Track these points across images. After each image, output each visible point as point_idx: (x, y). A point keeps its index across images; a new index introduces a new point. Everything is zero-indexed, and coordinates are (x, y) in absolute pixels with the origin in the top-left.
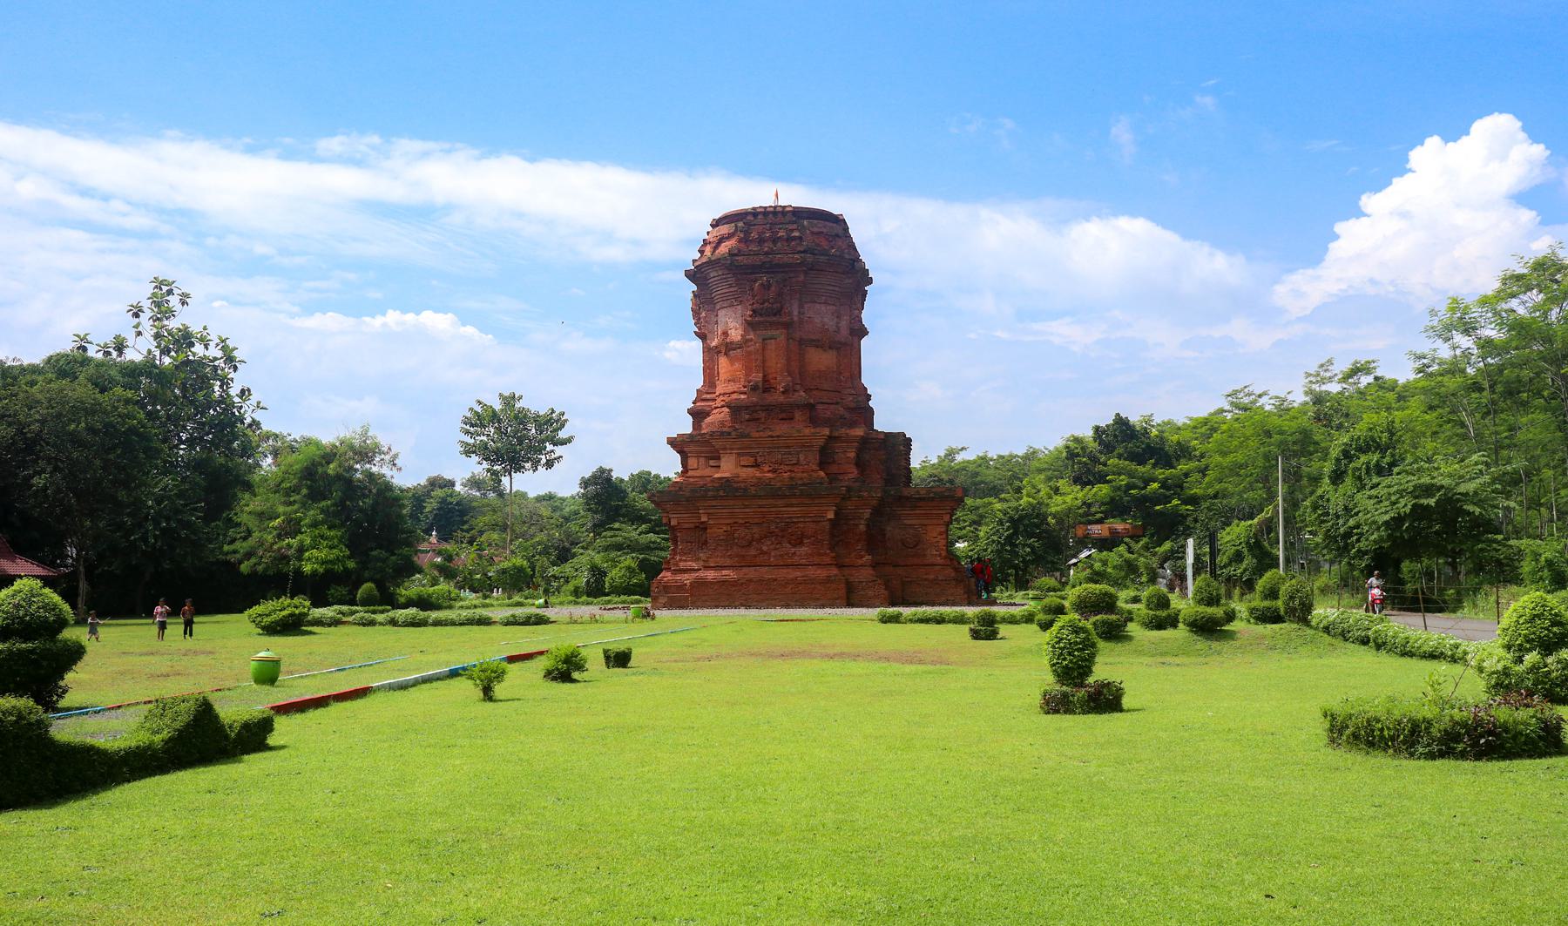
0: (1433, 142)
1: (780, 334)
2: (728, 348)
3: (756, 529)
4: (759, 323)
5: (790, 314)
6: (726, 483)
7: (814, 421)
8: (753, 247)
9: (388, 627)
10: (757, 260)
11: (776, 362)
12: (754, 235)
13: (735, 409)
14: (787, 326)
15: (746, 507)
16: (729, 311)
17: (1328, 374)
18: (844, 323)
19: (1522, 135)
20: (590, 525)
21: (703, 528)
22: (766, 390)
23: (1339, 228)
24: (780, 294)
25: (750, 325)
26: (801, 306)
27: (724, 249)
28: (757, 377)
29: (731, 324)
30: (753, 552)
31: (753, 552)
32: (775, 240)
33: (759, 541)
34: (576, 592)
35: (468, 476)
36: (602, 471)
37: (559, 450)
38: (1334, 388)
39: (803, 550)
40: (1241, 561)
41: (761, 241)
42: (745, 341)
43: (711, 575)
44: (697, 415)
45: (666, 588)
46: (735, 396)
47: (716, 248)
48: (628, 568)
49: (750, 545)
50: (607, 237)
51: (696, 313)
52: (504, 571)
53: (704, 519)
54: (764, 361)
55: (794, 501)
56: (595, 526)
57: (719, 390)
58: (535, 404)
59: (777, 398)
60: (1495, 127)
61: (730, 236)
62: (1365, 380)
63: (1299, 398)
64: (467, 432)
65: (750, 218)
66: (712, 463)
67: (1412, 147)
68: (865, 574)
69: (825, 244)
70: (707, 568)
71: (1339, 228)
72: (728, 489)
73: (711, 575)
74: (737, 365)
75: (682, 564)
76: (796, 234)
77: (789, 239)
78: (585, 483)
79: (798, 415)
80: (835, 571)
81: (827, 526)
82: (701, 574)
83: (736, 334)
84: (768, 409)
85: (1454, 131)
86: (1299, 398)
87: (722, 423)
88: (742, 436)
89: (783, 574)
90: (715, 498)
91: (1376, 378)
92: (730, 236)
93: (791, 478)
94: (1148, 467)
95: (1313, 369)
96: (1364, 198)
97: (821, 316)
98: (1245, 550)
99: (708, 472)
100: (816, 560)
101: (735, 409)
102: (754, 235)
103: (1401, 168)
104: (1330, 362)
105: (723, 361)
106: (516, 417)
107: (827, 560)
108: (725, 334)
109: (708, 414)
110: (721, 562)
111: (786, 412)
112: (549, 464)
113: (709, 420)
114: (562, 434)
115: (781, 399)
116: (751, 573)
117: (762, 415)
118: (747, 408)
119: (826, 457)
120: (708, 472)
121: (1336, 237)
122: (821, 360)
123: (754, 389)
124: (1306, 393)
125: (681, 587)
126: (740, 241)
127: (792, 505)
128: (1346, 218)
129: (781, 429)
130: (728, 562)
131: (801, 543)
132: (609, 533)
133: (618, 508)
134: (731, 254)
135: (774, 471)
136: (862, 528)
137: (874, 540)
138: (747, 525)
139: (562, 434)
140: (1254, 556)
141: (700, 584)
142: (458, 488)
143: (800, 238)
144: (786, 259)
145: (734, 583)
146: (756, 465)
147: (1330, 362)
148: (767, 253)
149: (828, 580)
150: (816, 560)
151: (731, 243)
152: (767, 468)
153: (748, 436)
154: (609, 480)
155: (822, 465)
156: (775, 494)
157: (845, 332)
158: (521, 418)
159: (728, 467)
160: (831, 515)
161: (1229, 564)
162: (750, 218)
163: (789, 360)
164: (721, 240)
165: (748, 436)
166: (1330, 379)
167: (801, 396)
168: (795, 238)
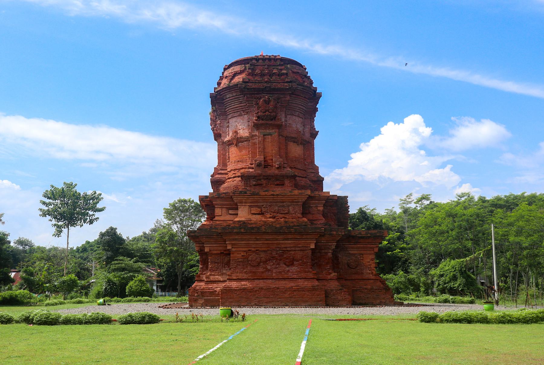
0: (391, 124)
1: (274, 132)
2: (237, 141)
3: (263, 255)
4: (262, 124)
5: (281, 119)
6: (243, 224)
7: (297, 186)
8: (258, 78)
9: (23, 325)
10: (261, 86)
11: (272, 149)
12: (258, 71)
13: (245, 178)
14: (279, 127)
15: (257, 240)
16: (239, 119)
17: (410, 200)
18: (307, 130)
19: (423, 124)
20: (105, 258)
21: (228, 253)
22: (266, 167)
23: (353, 155)
24: (276, 107)
25: (256, 126)
26: (286, 117)
27: (238, 79)
28: (260, 158)
29: (241, 126)
30: (261, 270)
31: (261, 270)
32: (271, 75)
33: (265, 262)
34: (98, 296)
35: (18, 239)
36: (112, 229)
37: (97, 215)
38: (413, 206)
39: (294, 269)
40: (456, 280)
41: (262, 75)
42: (252, 136)
43: (234, 285)
44: (216, 183)
45: (203, 293)
46: (242, 171)
47: (232, 79)
48: (140, 281)
49: (259, 265)
50: (61, 149)
51: (213, 121)
52: (64, 282)
53: (229, 247)
54: (264, 148)
55: (290, 236)
56: (108, 258)
57: (229, 168)
58: (83, 189)
59: (273, 171)
60: (414, 120)
61: (241, 72)
62: (426, 202)
63: (398, 211)
64: (44, 203)
65: (254, 61)
66: (231, 212)
67: (382, 126)
68: (334, 285)
69: (299, 79)
70: (230, 280)
71: (353, 155)
72: (245, 228)
73: (234, 285)
74: (244, 152)
75: (212, 278)
76: (285, 72)
77: (280, 75)
78: (102, 235)
79: (287, 182)
80: (316, 283)
81: (310, 253)
82: (228, 284)
83: (244, 132)
84: (268, 178)
85: (399, 120)
86: (398, 211)
87: (236, 187)
88: (253, 194)
89: (282, 284)
90: (238, 233)
91: (431, 202)
92: (241, 72)
93: (286, 222)
94: (131, 262)
95: (404, 197)
96: (362, 144)
97: (295, 123)
98: (458, 275)
99: (228, 217)
100: (303, 275)
101: (245, 178)
102: (258, 71)
103: (378, 133)
104: (411, 195)
105: (233, 151)
106: (74, 195)
107: (311, 275)
108: (236, 132)
109: (224, 182)
110: (240, 276)
111: (279, 180)
112: (91, 222)
113: (225, 185)
114: (99, 206)
115: (277, 172)
116: (261, 284)
117: (264, 182)
118: (254, 177)
119: (306, 211)
120: (228, 217)
121: (351, 158)
122: (296, 150)
123: (259, 165)
124: (401, 208)
125: (213, 293)
126: (249, 74)
127: (287, 239)
128: (355, 152)
129: (278, 190)
130: (245, 276)
131: (292, 265)
132: (116, 262)
133: (118, 249)
134: (244, 82)
135: (274, 217)
136: (330, 255)
137: (335, 264)
138: (257, 252)
139: (99, 206)
140: (463, 277)
141: (227, 291)
142: (12, 244)
143: (287, 74)
144: (279, 86)
145: (251, 290)
146: (262, 214)
147: (411, 195)
148: (266, 82)
149: (314, 289)
150: (303, 275)
151: (243, 76)
152: (268, 216)
153: (257, 194)
154: (115, 233)
155: (304, 214)
156: (278, 232)
157: (307, 135)
158: (77, 197)
159: (243, 214)
160: (313, 246)
161: (450, 282)
162: (254, 61)
163: (280, 148)
164: (235, 74)
165: (257, 194)
166: (410, 202)
167: (288, 171)
168: (283, 74)
